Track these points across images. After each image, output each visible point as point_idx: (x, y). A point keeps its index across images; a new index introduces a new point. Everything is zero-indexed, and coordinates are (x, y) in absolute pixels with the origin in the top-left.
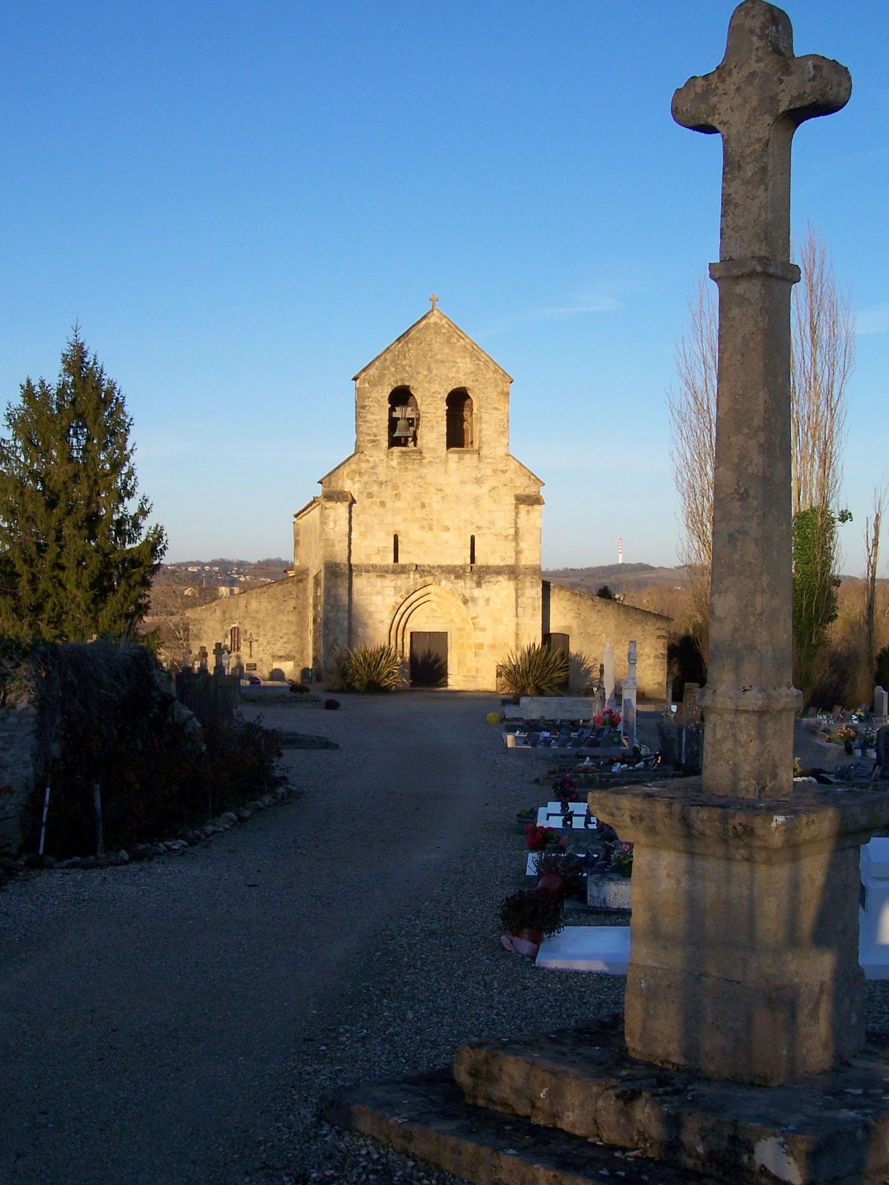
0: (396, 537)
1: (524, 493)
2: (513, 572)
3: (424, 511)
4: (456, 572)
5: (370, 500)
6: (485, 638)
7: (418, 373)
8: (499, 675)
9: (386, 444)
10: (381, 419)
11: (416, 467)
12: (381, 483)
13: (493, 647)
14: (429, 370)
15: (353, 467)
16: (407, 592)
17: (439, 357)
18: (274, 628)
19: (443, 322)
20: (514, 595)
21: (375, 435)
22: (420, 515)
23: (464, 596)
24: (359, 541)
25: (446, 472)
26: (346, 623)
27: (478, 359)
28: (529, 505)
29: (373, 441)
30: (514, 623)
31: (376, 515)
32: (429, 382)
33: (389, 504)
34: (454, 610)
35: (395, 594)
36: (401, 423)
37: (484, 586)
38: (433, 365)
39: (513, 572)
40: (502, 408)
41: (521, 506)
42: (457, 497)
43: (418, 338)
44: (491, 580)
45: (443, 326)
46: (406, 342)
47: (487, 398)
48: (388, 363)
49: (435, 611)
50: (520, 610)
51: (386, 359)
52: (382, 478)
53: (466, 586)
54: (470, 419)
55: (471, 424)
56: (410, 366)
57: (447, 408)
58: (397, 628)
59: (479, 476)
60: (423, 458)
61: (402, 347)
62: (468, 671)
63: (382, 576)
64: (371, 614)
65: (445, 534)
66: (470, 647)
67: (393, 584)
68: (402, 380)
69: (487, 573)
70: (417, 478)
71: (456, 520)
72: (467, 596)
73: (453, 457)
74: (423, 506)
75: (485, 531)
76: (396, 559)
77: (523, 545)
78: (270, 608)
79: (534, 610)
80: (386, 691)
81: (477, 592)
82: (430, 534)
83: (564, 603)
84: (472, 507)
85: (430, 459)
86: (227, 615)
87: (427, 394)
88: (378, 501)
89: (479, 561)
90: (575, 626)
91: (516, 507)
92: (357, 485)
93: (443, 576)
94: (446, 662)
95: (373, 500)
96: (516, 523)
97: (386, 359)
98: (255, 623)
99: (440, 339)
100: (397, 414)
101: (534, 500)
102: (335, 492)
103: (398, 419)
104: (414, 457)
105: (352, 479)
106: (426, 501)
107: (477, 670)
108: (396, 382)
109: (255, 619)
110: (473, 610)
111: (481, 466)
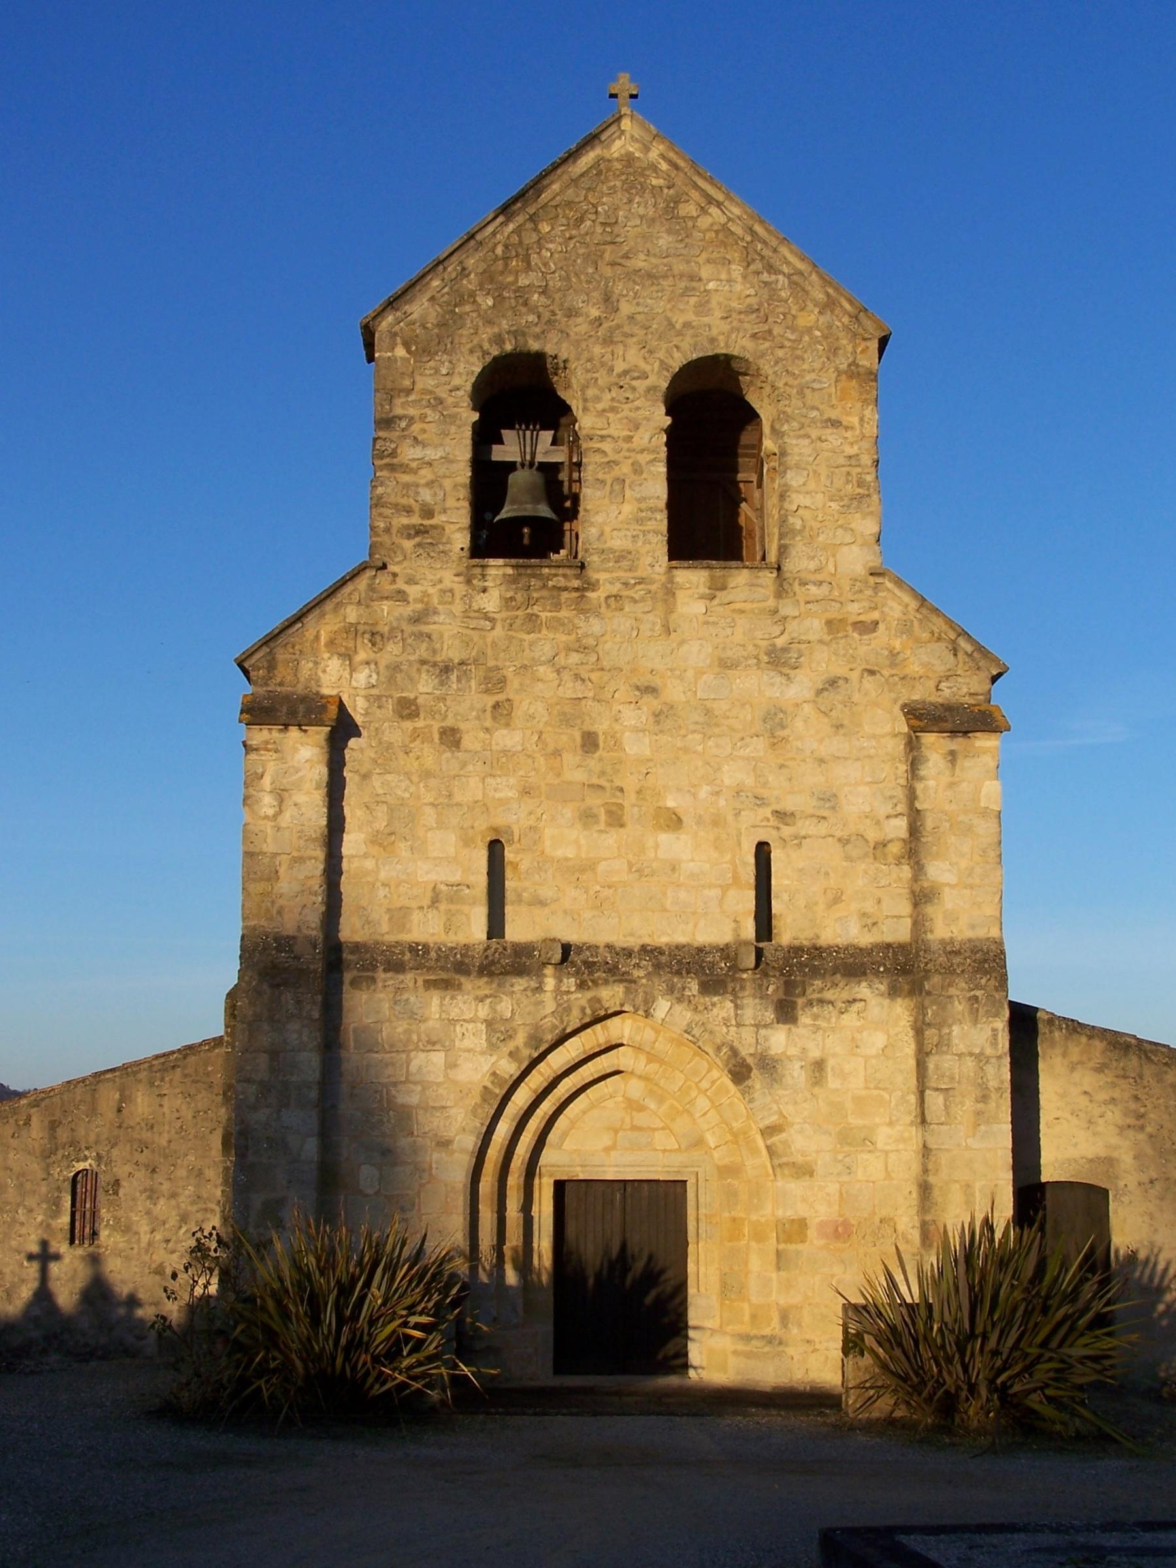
0: (495, 848)
1: (935, 698)
2: (905, 967)
3: (592, 762)
4: (703, 971)
5: (408, 725)
6: (814, 1202)
7: (571, 313)
8: (852, 1345)
9: (461, 540)
10: (447, 459)
11: (564, 613)
12: (447, 669)
13: (840, 1231)
14: (609, 301)
15: (352, 614)
16: (534, 1039)
17: (639, 262)
18: (200, 1173)
19: (654, 155)
20: (910, 1049)
21: (428, 513)
22: (579, 776)
23: (734, 1052)
24: (369, 864)
25: (667, 630)
26: (311, 1148)
27: (771, 269)
28: (954, 733)
29: (420, 531)
30: (915, 1145)
31: (427, 775)
32: (608, 341)
33: (471, 740)
34: (703, 1103)
35: (492, 1047)
36: (519, 480)
37: (805, 1019)
38: (619, 288)
39: (905, 967)
40: (855, 420)
41: (929, 739)
42: (708, 712)
43: (569, 204)
44: (829, 995)
45: (654, 168)
46: (533, 218)
47: (801, 393)
48: (470, 283)
49: (641, 1108)
50: (935, 1101)
51: (464, 272)
52: (452, 652)
53: (741, 1019)
54: (757, 494)
55: (760, 511)
56: (544, 292)
57: (668, 421)
58: (500, 1166)
59: (780, 642)
60: (592, 586)
61: (518, 231)
62: (754, 1317)
63: (446, 985)
64: (405, 1115)
65: (664, 838)
66: (759, 1236)
67: (483, 1011)
68: (515, 334)
69: (816, 972)
70: (569, 649)
71: (704, 791)
72: (745, 1052)
73: (693, 578)
74: (590, 742)
75: (806, 827)
76: (496, 926)
77: (938, 871)
78: (188, 1114)
79: (984, 1098)
80: (402, 1412)
81: (778, 1039)
82: (611, 839)
83: (1088, 1079)
84: (759, 746)
85: (615, 588)
86: (63, 1135)
87: (603, 378)
88: (436, 726)
89: (790, 929)
90: (1126, 1159)
91: (912, 745)
92: (362, 677)
93: (659, 985)
94: (682, 1287)
95: (420, 723)
96: (912, 796)
97: (464, 272)
98: (142, 1158)
99: (643, 207)
100: (508, 449)
101: (967, 721)
102: (287, 698)
103: (511, 467)
104: (562, 582)
105: (347, 656)
106: (601, 727)
107: (784, 1319)
108: (498, 340)
109: (144, 1146)
110: (768, 1101)
111: (787, 609)
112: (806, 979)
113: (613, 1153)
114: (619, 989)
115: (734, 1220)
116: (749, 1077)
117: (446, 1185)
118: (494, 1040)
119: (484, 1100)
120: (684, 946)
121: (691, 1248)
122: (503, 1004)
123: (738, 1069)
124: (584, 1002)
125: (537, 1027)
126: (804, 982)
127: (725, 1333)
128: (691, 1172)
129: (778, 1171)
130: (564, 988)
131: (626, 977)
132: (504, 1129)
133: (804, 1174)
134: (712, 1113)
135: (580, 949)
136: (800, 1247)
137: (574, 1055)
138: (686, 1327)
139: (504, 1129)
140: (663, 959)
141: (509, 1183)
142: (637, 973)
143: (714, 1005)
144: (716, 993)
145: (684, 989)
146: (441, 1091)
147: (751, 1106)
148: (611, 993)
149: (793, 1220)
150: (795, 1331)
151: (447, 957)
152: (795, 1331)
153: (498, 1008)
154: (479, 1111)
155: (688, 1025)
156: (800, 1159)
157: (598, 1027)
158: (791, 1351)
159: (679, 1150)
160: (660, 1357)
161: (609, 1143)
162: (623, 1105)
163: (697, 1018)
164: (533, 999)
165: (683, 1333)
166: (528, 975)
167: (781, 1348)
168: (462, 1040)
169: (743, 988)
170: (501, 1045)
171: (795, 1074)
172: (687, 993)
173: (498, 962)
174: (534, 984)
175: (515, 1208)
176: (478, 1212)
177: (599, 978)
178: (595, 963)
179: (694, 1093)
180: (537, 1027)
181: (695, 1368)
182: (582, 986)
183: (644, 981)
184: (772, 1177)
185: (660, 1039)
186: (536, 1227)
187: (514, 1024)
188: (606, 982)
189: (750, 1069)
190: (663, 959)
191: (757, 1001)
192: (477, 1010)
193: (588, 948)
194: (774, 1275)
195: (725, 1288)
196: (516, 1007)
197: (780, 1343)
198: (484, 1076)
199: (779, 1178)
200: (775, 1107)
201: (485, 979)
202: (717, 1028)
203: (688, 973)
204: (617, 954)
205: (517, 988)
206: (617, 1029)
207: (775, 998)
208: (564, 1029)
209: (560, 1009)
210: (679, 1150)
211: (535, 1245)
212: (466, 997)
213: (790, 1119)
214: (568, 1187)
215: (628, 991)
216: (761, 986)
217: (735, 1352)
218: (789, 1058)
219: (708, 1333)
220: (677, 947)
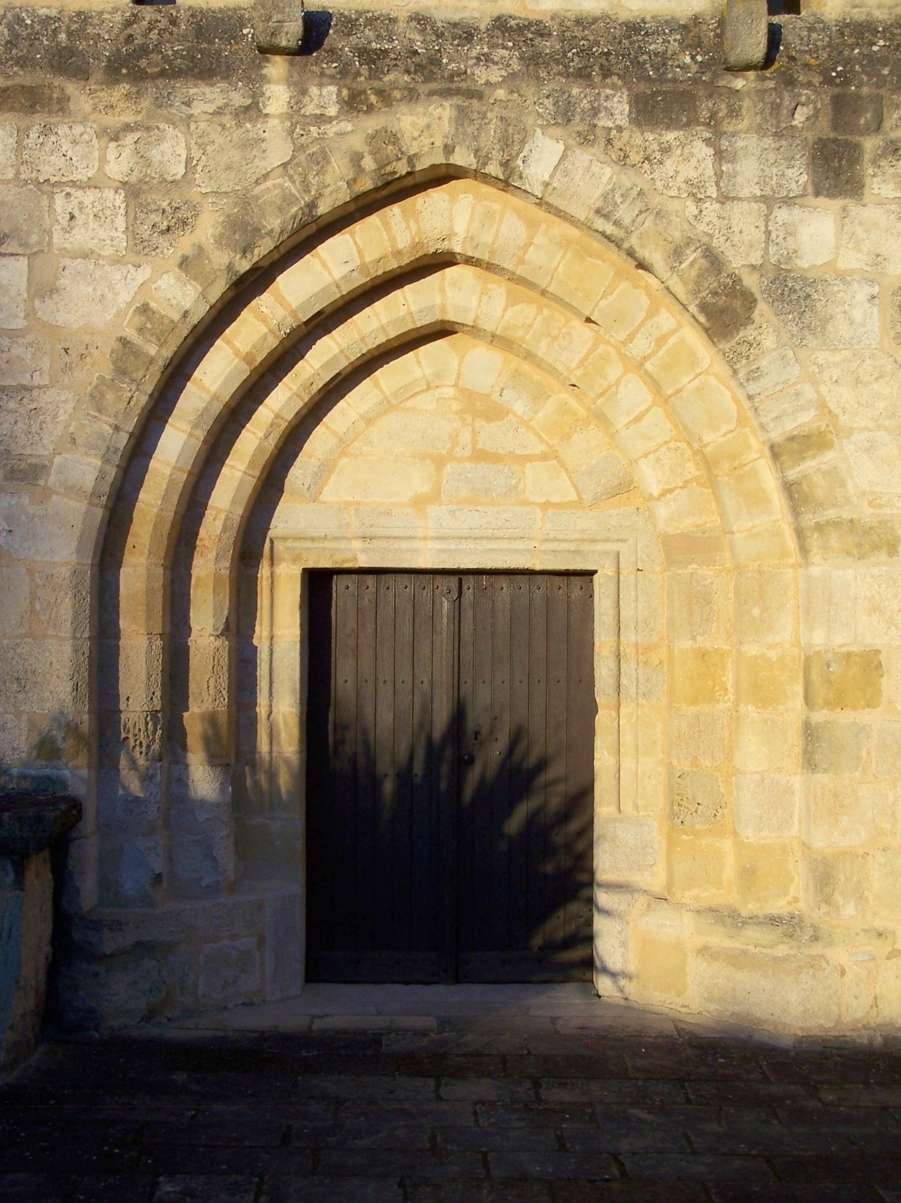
23: (714, 261)
35: (140, 247)
37: (881, 184)
49: (495, 413)
62: (748, 874)
66: (761, 690)
67: (119, 163)
81: (818, 233)
93: (536, 102)
94: (581, 799)
107: (824, 878)
110: (793, 377)
112: (883, 92)
113: (433, 511)
114: (443, 113)
115: (702, 655)
116: (749, 320)
117: (30, 572)
118: (144, 230)
119: (121, 372)
120: (595, 20)
121: (603, 720)
122: (166, 146)
123: (722, 300)
124: (357, 142)
125: (246, 201)
126: (878, 100)
127: (680, 906)
128: (606, 553)
129: (814, 541)
130: (310, 109)
131: (458, 84)
132: (176, 445)
133: (876, 547)
134: (657, 415)
135: (350, 24)
136: (864, 716)
137: (337, 275)
138: (590, 883)
139: (176, 445)
140: (547, 46)
141: (195, 572)
142: (483, 75)
143: (666, 150)
144: (671, 124)
145: (595, 111)
146: (17, 350)
147: (752, 388)
148: (422, 122)
149: (849, 656)
150: (849, 910)
151: (34, 37)
152: (849, 910)
153: (155, 154)
154: (110, 397)
155: (605, 196)
156: (866, 514)
157: (395, 211)
158: (839, 955)
159: (578, 504)
160: (537, 941)
161: (425, 488)
162: (456, 406)
163: (627, 179)
164: (237, 134)
165: (584, 893)
166: (226, 77)
167: (816, 949)
168: (67, 231)
169: (734, 113)
170: (162, 242)
171: (857, 315)
172: (603, 122)
173: (157, 49)
174: (239, 99)
175: (210, 630)
176: (117, 635)
177: (394, 86)
178: (385, 52)
179: (614, 372)
180: (246, 201)
181: (613, 975)
182: (353, 103)
183: (501, 93)
184: (795, 557)
185: (538, 239)
186: (262, 671)
187: (193, 194)
188: (412, 96)
189: (750, 302)
190: (547, 46)
191: (768, 142)
192: (103, 160)
193: (372, 21)
194: (797, 781)
195: (679, 808)
196: (196, 153)
197: (815, 938)
198: (120, 314)
199: (816, 556)
200: (809, 393)
201: (125, 88)
202: (674, 206)
203: (606, 73)
204: (439, 35)
205: (198, 108)
206: (441, 216)
207: (811, 137)
208: (312, 206)
209: (302, 157)
210: (578, 504)
211: (262, 710)
212: (78, 129)
213: (843, 419)
214: (339, 585)
215: (462, 115)
216: (776, 108)
217: (704, 951)
218: (843, 277)
219: (642, 901)
220: (578, 22)
